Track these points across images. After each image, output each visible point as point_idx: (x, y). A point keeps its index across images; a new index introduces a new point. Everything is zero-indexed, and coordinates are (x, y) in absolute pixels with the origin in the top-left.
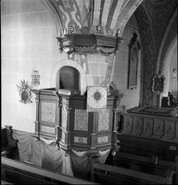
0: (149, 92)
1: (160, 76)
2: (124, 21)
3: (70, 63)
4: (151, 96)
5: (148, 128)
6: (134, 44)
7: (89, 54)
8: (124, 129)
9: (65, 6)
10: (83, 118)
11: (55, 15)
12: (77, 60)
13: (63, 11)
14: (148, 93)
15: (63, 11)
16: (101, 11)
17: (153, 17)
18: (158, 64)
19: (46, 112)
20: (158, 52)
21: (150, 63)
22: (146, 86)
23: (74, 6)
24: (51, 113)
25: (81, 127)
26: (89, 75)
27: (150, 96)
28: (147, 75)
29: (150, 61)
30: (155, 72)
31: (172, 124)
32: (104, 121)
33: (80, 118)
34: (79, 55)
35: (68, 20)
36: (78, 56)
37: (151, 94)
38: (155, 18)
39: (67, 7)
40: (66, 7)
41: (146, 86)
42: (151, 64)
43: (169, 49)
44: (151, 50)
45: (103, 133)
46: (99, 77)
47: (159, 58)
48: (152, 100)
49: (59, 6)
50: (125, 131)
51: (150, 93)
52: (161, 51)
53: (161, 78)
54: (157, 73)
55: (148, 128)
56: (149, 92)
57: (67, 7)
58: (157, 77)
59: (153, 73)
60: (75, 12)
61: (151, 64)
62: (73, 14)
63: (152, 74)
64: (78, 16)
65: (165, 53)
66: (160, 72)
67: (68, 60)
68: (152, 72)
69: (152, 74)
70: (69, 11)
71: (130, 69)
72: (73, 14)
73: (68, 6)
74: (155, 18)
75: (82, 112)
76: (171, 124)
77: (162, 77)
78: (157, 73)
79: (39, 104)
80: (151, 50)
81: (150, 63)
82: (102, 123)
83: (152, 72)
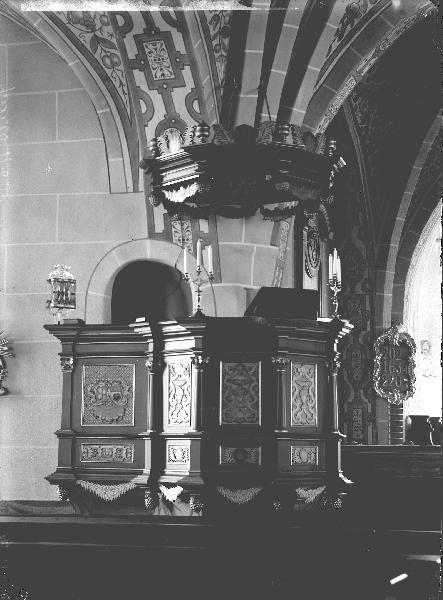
0: (363, 397)
1: (397, 336)
2: (321, 124)
3: (152, 251)
4: (370, 411)
7: (222, 218)
9: (154, 72)
10: (246, 387)
11: (104, 103)
12: (183, 240)
13: (144, 87)
15: (144, 87)
16: (262, 91)
17: (366, 129)
18: (388, 295)
19: (100, 396)
20: (386, 250)
23: (187, 72)
24: (117, 398)
25: (240, 415)
26: (220, 285)
27: (364, 410)
30: (381, 324)
32: (304, 398)
33: (234, 387)
34: (187, 224)
35: (160, 114)
36: (185, 226)
37: (370, 405)
38: (369, 133)
39: (163, 75)
40: (159, 74)
43: (420, 242)
44: (359, 244)
45: (300, 436)
46: (251, 292)
47: (390, 273)
48: (375, 427)
49: (136, 72)
51: (366, 401)
52: (395, 246)
53: (403, 344)
54: (387, 325)
56: (363, 397)
57: (163, 75)
59: (372, 324)
60: (187, 90)
62: (179, 96)
63: (369, 328)
64: (196, 102)
65: (375, 285)
66: (397, 320)
67: (148, 241)
69: (369, 328)
70: (165, 88)
71: (36, 499)
72: (179, 96)
73: (166, 72)
74: (369, 133)
75: (240, 368)
77: (405, 341)
78: (387, 325)
79: (73, 370)
80: (359, 244)
82: (298, 404)
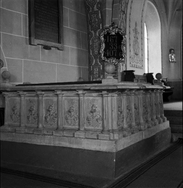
0: (98, 62)
4: (101, 69)
5: (14, 113)
6: (133, 71)
8: (6, 123)
14: (96, 63)
21: (96, 9)
22: (93, 52)
27: (99, 68)
28: (92, 32)
29: (95, 6)
31: (97, 98)
41: (93, 52)
42: (98, 10)
50: (9, 126)
51: (100, 64)
55: (14, 113)
56: (98, 62)
58: (107, 31)
59: (102, 27)
61: (98, 10)
63: (101, 28)
68: (101, 25)
69: (101, 28)
76: (93, 100)
81: (96, 9)
83: (101, 25)
